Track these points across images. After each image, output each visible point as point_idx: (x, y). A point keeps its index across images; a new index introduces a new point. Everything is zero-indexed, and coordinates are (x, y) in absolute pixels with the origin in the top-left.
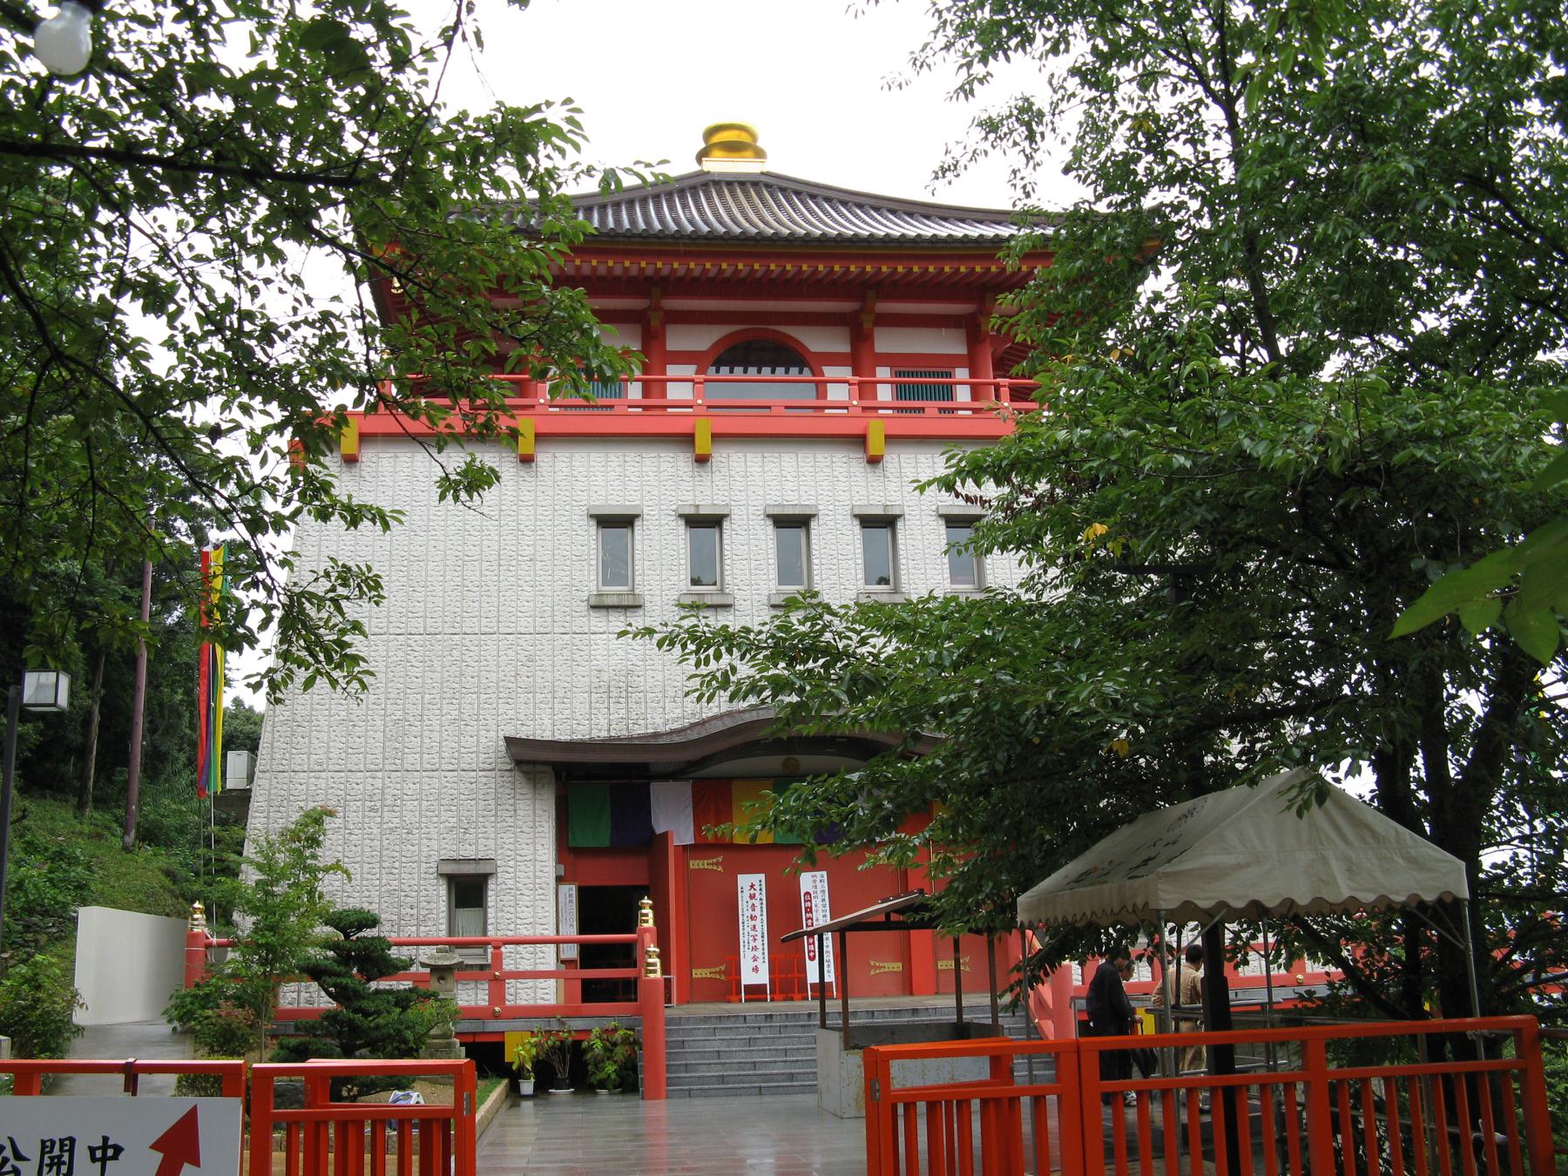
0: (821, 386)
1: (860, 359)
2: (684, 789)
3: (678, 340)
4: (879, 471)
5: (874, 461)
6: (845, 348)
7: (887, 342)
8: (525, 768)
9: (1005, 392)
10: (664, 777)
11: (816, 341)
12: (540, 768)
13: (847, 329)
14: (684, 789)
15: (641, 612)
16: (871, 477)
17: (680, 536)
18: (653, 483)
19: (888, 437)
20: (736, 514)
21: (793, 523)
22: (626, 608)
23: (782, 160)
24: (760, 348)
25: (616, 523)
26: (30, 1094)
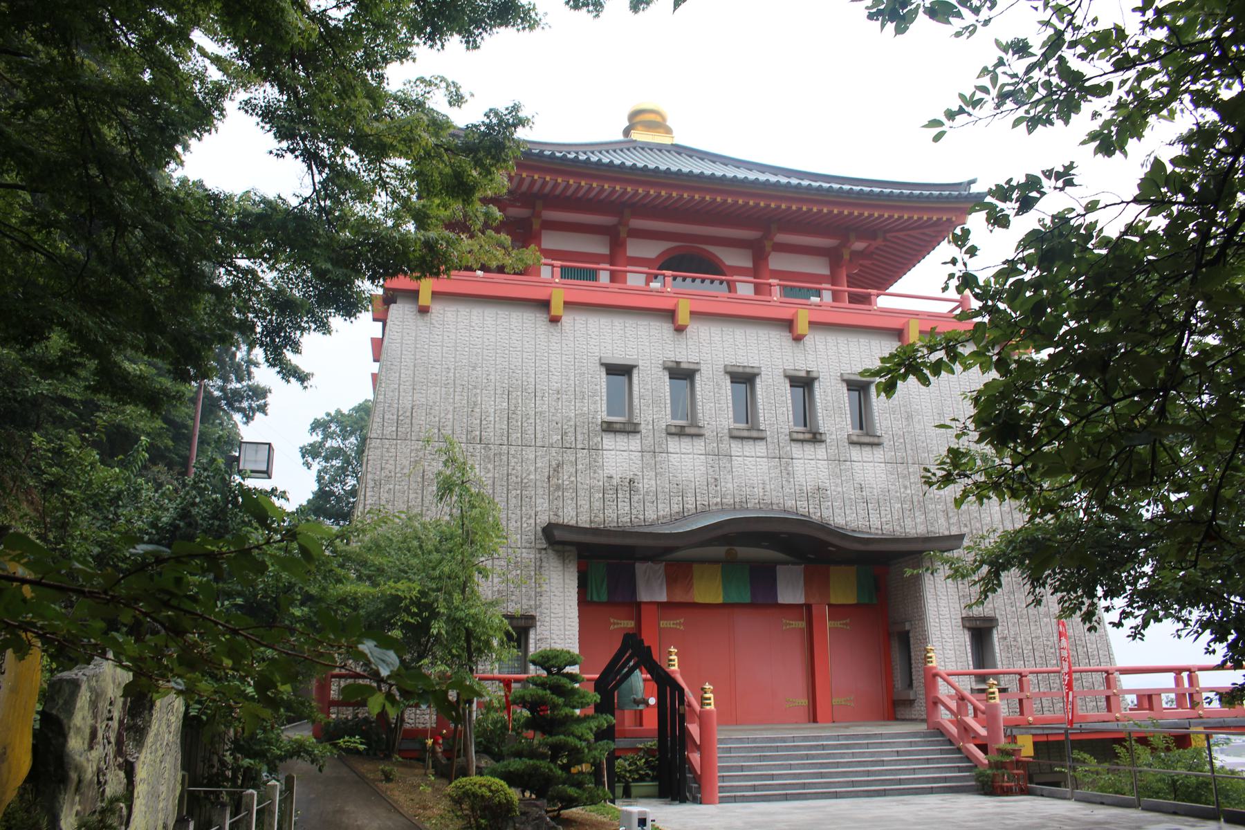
0: (731, 287)
1: (758, 269)
2: (660, 568)
3: (635, 249)
4: (801, 345)
5: (555, 320)
6: (749, 264)
7: (777, 262)
8: (557, 547)
9: (557, 270)
10: (645, 559)
11: (730, 258)
12: (568, 548)
13: (608, 238)
14: (660, 568)
15: (639, 436)
16: (420, 322)
17: (844, 396)
18: (644, 344)
19: (810, 323)
20: (703, 367)
21: (744, 379)
22: (628, 432)
23: (680, 138)
24: (689, 260)
25: (620, 371)
26: (683, 800)
